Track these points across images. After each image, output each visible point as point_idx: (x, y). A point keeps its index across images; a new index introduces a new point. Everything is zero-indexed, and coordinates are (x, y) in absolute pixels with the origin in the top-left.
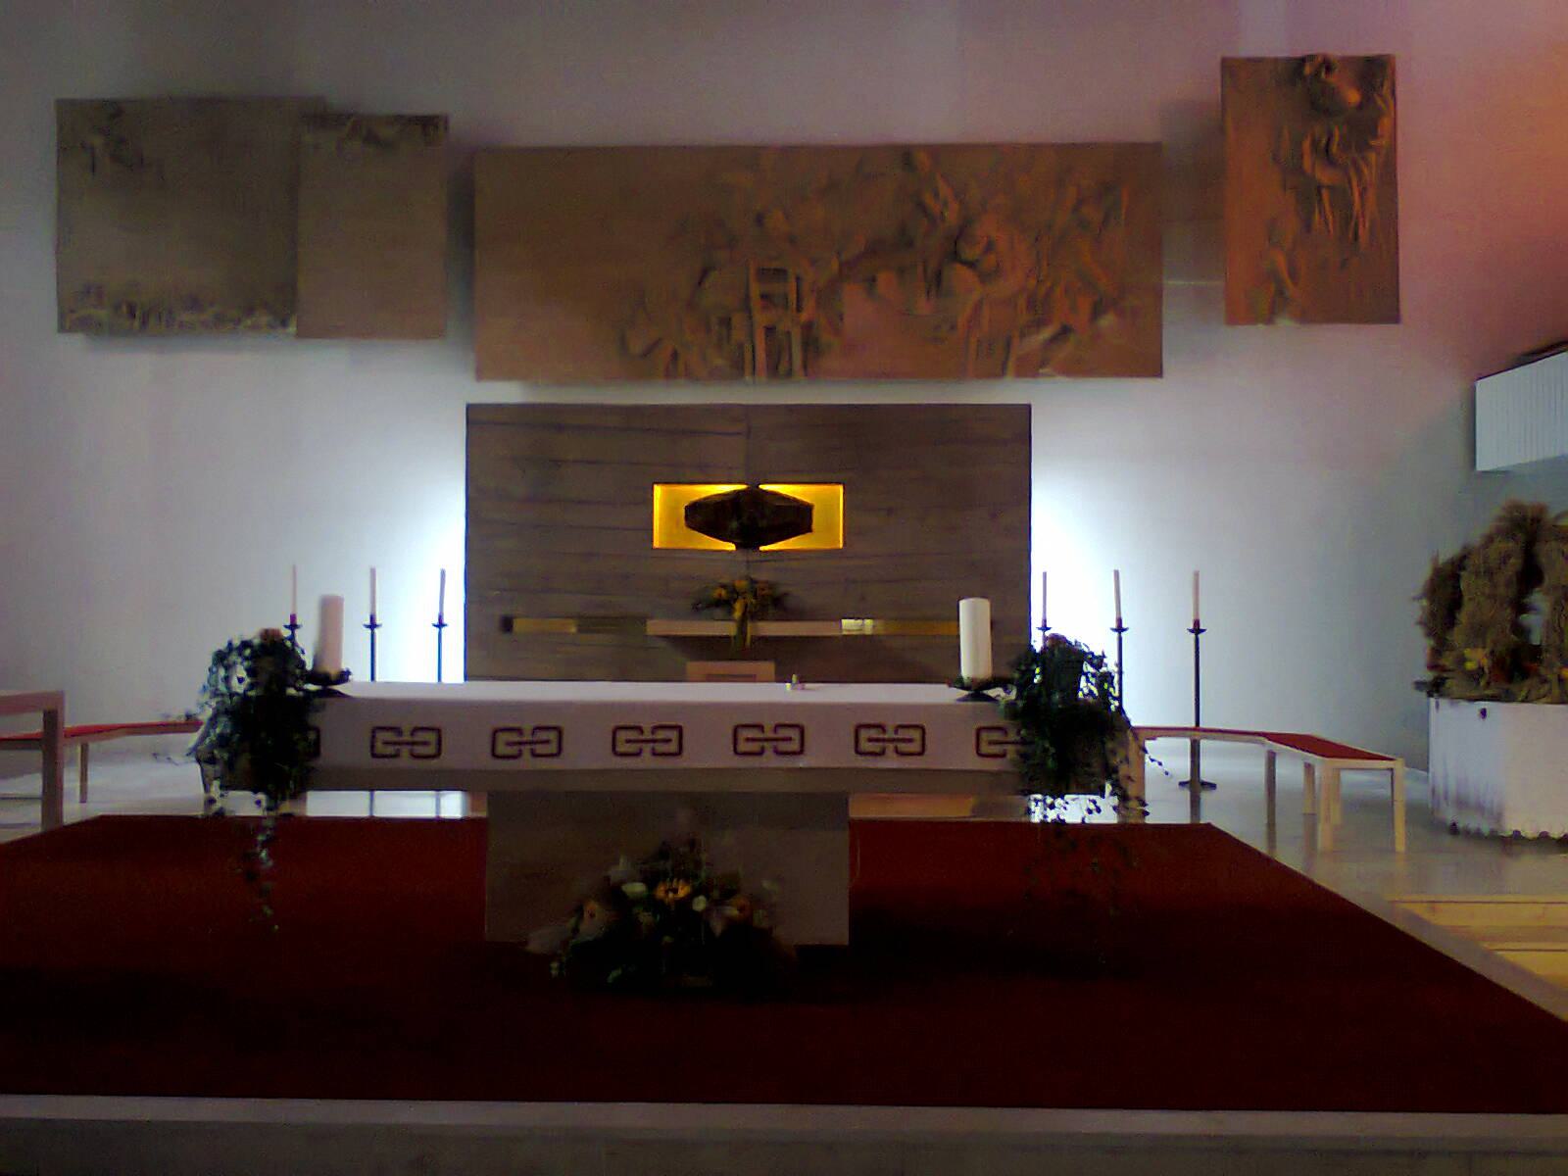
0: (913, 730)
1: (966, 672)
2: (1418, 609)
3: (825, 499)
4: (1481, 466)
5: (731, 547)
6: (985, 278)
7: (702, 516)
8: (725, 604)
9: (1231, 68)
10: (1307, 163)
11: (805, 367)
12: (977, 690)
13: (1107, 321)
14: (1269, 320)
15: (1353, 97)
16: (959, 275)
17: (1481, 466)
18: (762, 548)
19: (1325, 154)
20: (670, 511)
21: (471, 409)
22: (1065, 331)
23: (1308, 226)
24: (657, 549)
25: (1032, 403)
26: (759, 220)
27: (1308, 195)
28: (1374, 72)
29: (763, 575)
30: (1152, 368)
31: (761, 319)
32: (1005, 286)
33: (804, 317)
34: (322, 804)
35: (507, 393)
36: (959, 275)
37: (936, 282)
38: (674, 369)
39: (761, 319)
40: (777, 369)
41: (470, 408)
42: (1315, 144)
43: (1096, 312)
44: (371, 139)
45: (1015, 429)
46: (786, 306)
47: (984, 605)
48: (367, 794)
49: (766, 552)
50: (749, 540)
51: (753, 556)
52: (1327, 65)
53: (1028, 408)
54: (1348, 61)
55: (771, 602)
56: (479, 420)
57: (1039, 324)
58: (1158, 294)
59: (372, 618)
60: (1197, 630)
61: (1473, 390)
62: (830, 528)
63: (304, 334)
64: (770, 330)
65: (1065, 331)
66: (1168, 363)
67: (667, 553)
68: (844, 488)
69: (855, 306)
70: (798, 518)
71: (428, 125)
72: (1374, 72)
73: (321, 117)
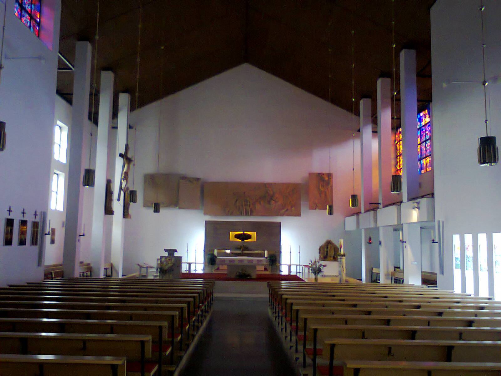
0: (261, 261)
1: (265, 256)
2: (318, 251)
3: (254, 234)
4: (346, 229)
5: (240, 240)
6: (276, 202)
7: (237, 236)
8: (240, 249)
9: (311, 174)
10: (320, 187)
11: (251, 214)
12: (266, 258)
13: (293, 208)
14: (315, 209)
15: (327, 179)
16: (273, 202)
17: (347, 229)
18: (245, 241)
19: (323, 186)
20: (232, 235)
22: (287, 210)
23: (321, 196)
26: (244, 193)
27: (320, 193)
28: (329, 175)
29: (245, 244)
30: (299, 215)
31: (244, 207)
32: (279, 203)
33: (251, 207)
34: (242, 232)
35: (209, 218)
36: (273, 202)
37: (269, 202)
38: (232, 214)
39: (244, 207)
40: (247, 214)
41: (206, 221)
42: (321, 185)
43: (292, 207)
44: (190, 181)
45: (278, 226)
46: (248, 206)
47: (267, 251)
50: (243, 240)
51: (243, 242)
52: (323, 174)
53: (280, 223)
55: (246, 248)
56: (207, 223)
57: (283, 209)
58: (300, 205)
59: (187, 250)
60: (299, 253)
62: (254, 239)
63: (180, 208)
64: (246, 209)
65: (287, 210)
66: (302, 214)
67: (233, 242)
68: (256, 233)
69: (258, 207)
70: (249, 237)
71: (198, 179)
72: (329, 175)
73: (184, 178)
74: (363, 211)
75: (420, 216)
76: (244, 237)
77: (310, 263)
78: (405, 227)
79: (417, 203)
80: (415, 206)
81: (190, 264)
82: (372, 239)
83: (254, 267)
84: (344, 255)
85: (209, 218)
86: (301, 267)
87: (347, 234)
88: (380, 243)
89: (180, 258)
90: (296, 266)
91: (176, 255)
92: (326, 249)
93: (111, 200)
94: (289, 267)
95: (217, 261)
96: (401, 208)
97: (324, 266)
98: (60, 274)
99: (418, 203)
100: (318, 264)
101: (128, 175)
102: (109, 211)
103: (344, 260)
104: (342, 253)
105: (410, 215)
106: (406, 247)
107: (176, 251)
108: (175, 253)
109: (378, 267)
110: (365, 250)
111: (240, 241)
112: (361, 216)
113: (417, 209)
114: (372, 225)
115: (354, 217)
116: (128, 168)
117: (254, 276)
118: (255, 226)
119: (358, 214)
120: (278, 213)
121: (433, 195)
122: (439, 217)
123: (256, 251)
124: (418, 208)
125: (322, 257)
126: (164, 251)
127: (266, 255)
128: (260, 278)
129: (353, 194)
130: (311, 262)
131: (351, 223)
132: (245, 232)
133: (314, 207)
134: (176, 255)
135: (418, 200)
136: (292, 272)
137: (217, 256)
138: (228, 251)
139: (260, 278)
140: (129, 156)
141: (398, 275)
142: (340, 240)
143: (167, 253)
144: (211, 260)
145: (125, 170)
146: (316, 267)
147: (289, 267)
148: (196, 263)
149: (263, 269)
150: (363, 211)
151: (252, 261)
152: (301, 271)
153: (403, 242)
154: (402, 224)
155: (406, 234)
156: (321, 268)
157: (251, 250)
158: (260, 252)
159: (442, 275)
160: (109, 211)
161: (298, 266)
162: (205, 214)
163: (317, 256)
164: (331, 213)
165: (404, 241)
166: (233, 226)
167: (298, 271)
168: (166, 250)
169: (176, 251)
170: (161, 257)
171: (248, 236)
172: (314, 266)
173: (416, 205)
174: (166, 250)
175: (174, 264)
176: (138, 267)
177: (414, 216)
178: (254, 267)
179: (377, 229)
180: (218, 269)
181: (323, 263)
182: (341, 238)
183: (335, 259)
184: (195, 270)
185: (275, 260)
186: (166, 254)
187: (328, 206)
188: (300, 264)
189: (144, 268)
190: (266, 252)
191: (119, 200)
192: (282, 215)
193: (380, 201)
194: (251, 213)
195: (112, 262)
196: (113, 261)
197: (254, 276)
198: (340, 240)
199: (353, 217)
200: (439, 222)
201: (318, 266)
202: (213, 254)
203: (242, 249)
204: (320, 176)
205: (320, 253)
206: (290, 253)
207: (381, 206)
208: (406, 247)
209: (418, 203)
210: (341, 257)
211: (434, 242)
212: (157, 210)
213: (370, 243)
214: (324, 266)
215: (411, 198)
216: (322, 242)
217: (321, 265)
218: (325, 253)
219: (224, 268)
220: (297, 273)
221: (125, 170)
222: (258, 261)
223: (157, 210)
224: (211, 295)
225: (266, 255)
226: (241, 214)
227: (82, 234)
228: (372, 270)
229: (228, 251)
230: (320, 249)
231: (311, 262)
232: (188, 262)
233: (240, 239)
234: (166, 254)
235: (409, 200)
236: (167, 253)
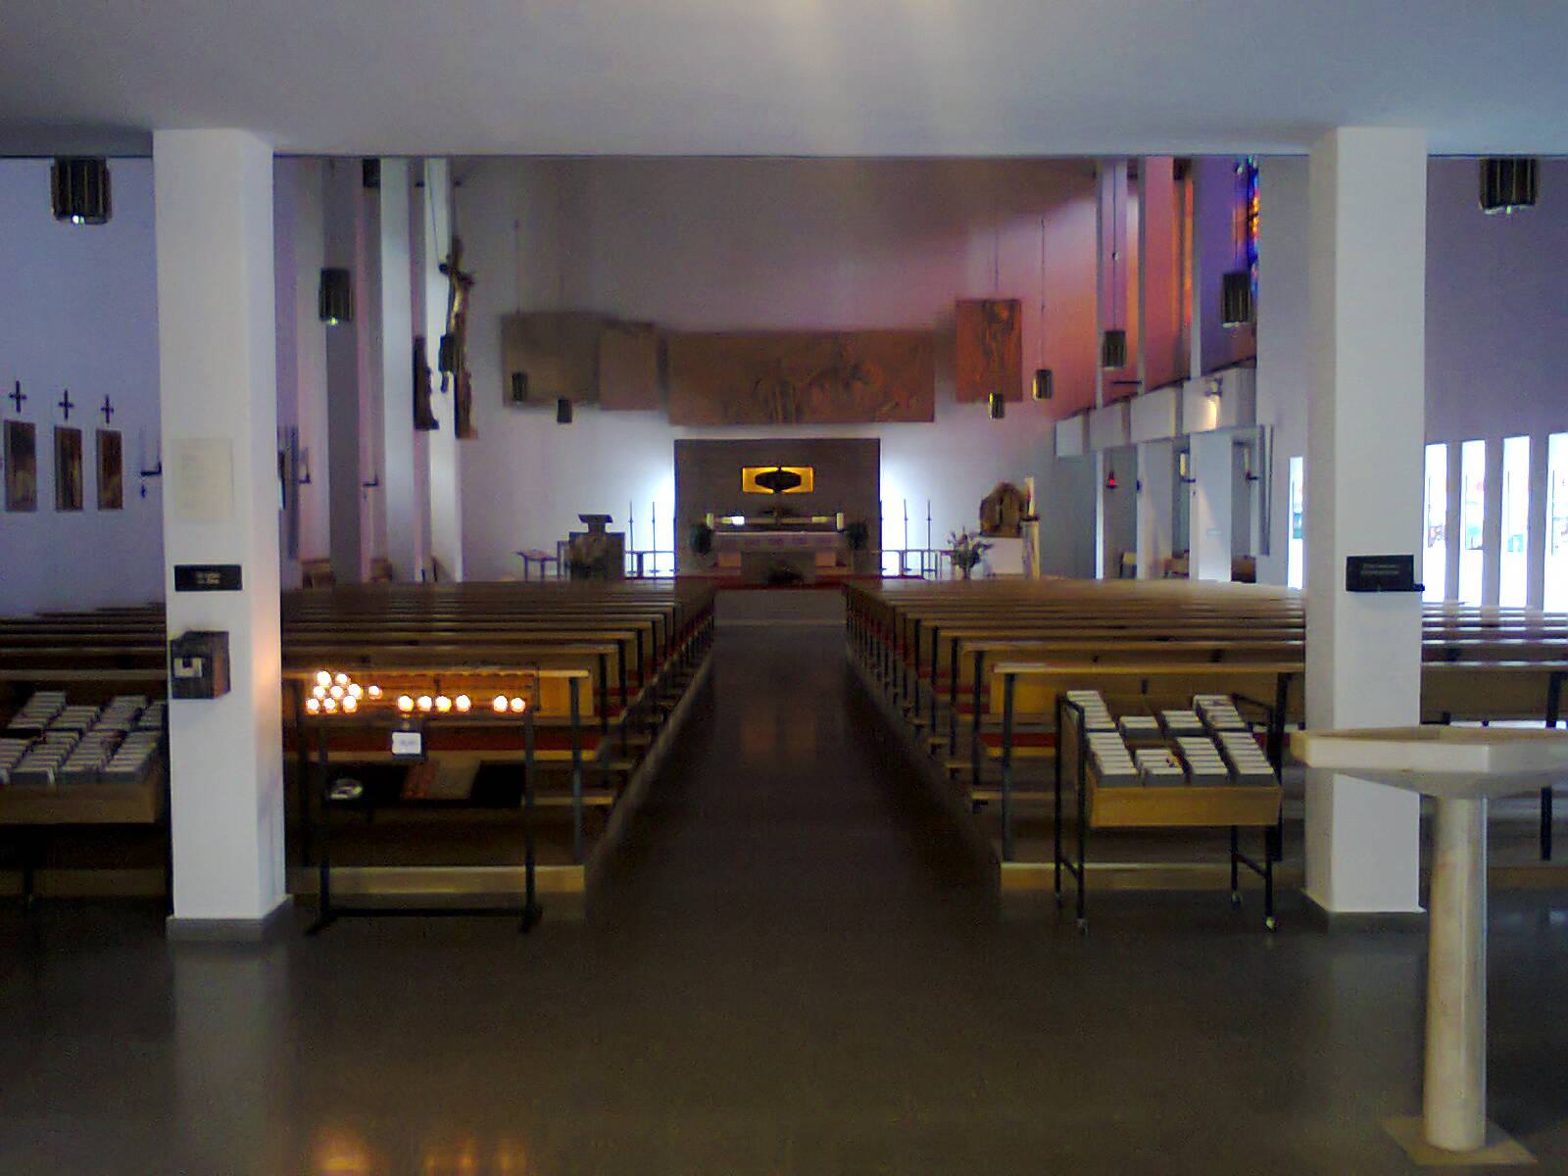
0: (828, 540)
2: (978, 512)
3: (806, 473)
4: (1060, 454)
5: (771, 491)
7: (762, 480)
8: (768, 513)
12: (842, 531)
13: (913, 401)
15: (1005, 315)
17: (1060, 454)
21: (676, 442)
24: (999, 867)
25: (881, 438)
28: (1014, 305)
30: (932, 419)
34: (775, 469)
35: (682, 433)
37: (847, 386)
38: (741, 420)
40: (786, 420)
41: (676, 442)
45: (874, 447)
48: (672, 549)
49: (787, 494)
50: (778, 488)
53: (879, 440)
54: (1005, 301)
55: (786, 512)
56: (679, 446)
60: (929, 519)
61: (1055, 428)
66: (938, 416)
68: (814, 473)
70: (796, 480)
71: (649, 326)
72: (1014, 305)
73: (612, 323)
74: (1100, 401)
75: (1223, 411)
76: (779, 481)
77: (951, 538)
78: (1194, 444)
79: (1215, 380)
80: (1211, 389)
81: (640, 556)
82: (1117, 475)
83: (809, 556)
84: (1036, 518)
85: (682, 433)
86: (933, 555)
87: (1059, 469)
88: (1138, 486)
89: (619, 538)
90: (920, 553)
91: (609, 528)
92: (998, 508)
93: (428, 390)
94: (903, 554)
95: (714, 543)
96: (1259, 379)
97: (986, 547)
98: (329, 578)
99: (1220, 382)
100: (971, 544)
101: (463, 322)
102: (424, 420)
103: (1035, 529)
104: (1031, 512)
105: (1201, 412)
106: (1194, 493)
107: (609, 519)
108: (608, 525)
109: (1133, 549)
110: (382, 365)
111: (768, 494)
112: (1094, 416)
113: (1217, 398)
114: (1119, 441)
115: (1078, 420)
116: (465, 302)
117: (810, 579)
118: (808, 452)
119: (1087, 410)
120: (874, 416)
121: (1252, 359)
122: (1264, 416)
123: (815, 519)
124: (1219, 393)
125: (986, 526)
126: (579, 520)
127: (840, 525)
128: (826, 584)
129: (1040, 367)
130: (954, 536)
131: (1069, 436)
132: (784, 469)
133: (969, 394)
134: (609, 528)
135: (1218, 375)
136: (909, 570)
137: (714, 531)
138: (739, 521)
139: (826, 584)
140: (464, 268)
141: (1179, 567)
142: (1026, 480)
143: (586, 525)
144: (694, 538)
145: (456, 308)
146: (966, 551)
147: (903, 554)
148: (654, 552)
149: (833, 564)
150: (1100, 401)
151: (802, 540)
152: (933, 568)
153: (1189, 481)
154: (1188, 437)
155: (1196, 463)
156: (980, 551)
157: (798, 516)
158: (823, 519)
159: (1265, 557)
160: (424, 420)
161: (926, 555)
162: (675, 421)
163: (975, 524)
164: (998, 412)
165: (1192, 478)
166: (751, 453)
167: (926, 567)
168: (584, 519)
169: (609, 519)
170: (572, 535)
171: (364, 661)
172: (961, 548)
173: (1214, 387)
174: (584, 519)
175: (607, 552)
176: (522, 558)
177: (1211, 413)
178: (809, 556)
179: (1131, 449)
180: (715, 565)
181: (985, 541)
182: (1028, 475)
183: (1018, 532)
184: (655, 571)
185: (865, 534)
186: (584, 528)
187: (991, 397)
188: (932, 548)
189: (533, 560)
190: (840, 517)
191: (444, 388)
192: (884, 419)
193: (1141, 375)
194: (795, 416)
195: (434, 554)
196: (438, 552)
197: (810, 579)
198: (1026, 480)
199: (1076, 419)
200: (1263, 428)
201: (970, 547)
202: (703, 526)
203: (775, 514)
204: (987, 307)
205: (982, 516)
206: (906, 519)
207: (1141, 389)
208: (1194, 493)
209: (1220, 382)
210: (1029, 523)
211: (1249, 477)
212: (564, 417)
213: (1112, 487)
214: (986, 547)
215: (1209, 370)
216: (988, 490)
217: (979, 545)
218: (997, 516)
219: (731, 563)
220: (923, 570)
221: (456, 308)
222: (822, 540)
223: (564, 417)
224: (693, 643)
225: (840, 525)
226: (770, 420)
227: (371, 481)
228: (1122, 557)
229: (739, 521)
230: (984, 503)
231: (954, 536)
232: (635, 549)
233: (770, 488)
234: (584, 528)
235: (1204, 373)
236: (586, 525)
